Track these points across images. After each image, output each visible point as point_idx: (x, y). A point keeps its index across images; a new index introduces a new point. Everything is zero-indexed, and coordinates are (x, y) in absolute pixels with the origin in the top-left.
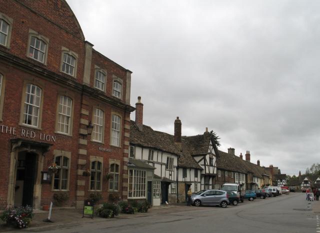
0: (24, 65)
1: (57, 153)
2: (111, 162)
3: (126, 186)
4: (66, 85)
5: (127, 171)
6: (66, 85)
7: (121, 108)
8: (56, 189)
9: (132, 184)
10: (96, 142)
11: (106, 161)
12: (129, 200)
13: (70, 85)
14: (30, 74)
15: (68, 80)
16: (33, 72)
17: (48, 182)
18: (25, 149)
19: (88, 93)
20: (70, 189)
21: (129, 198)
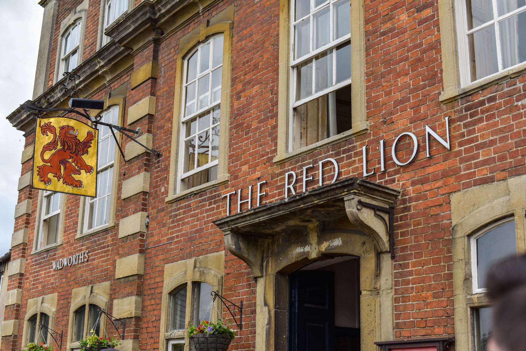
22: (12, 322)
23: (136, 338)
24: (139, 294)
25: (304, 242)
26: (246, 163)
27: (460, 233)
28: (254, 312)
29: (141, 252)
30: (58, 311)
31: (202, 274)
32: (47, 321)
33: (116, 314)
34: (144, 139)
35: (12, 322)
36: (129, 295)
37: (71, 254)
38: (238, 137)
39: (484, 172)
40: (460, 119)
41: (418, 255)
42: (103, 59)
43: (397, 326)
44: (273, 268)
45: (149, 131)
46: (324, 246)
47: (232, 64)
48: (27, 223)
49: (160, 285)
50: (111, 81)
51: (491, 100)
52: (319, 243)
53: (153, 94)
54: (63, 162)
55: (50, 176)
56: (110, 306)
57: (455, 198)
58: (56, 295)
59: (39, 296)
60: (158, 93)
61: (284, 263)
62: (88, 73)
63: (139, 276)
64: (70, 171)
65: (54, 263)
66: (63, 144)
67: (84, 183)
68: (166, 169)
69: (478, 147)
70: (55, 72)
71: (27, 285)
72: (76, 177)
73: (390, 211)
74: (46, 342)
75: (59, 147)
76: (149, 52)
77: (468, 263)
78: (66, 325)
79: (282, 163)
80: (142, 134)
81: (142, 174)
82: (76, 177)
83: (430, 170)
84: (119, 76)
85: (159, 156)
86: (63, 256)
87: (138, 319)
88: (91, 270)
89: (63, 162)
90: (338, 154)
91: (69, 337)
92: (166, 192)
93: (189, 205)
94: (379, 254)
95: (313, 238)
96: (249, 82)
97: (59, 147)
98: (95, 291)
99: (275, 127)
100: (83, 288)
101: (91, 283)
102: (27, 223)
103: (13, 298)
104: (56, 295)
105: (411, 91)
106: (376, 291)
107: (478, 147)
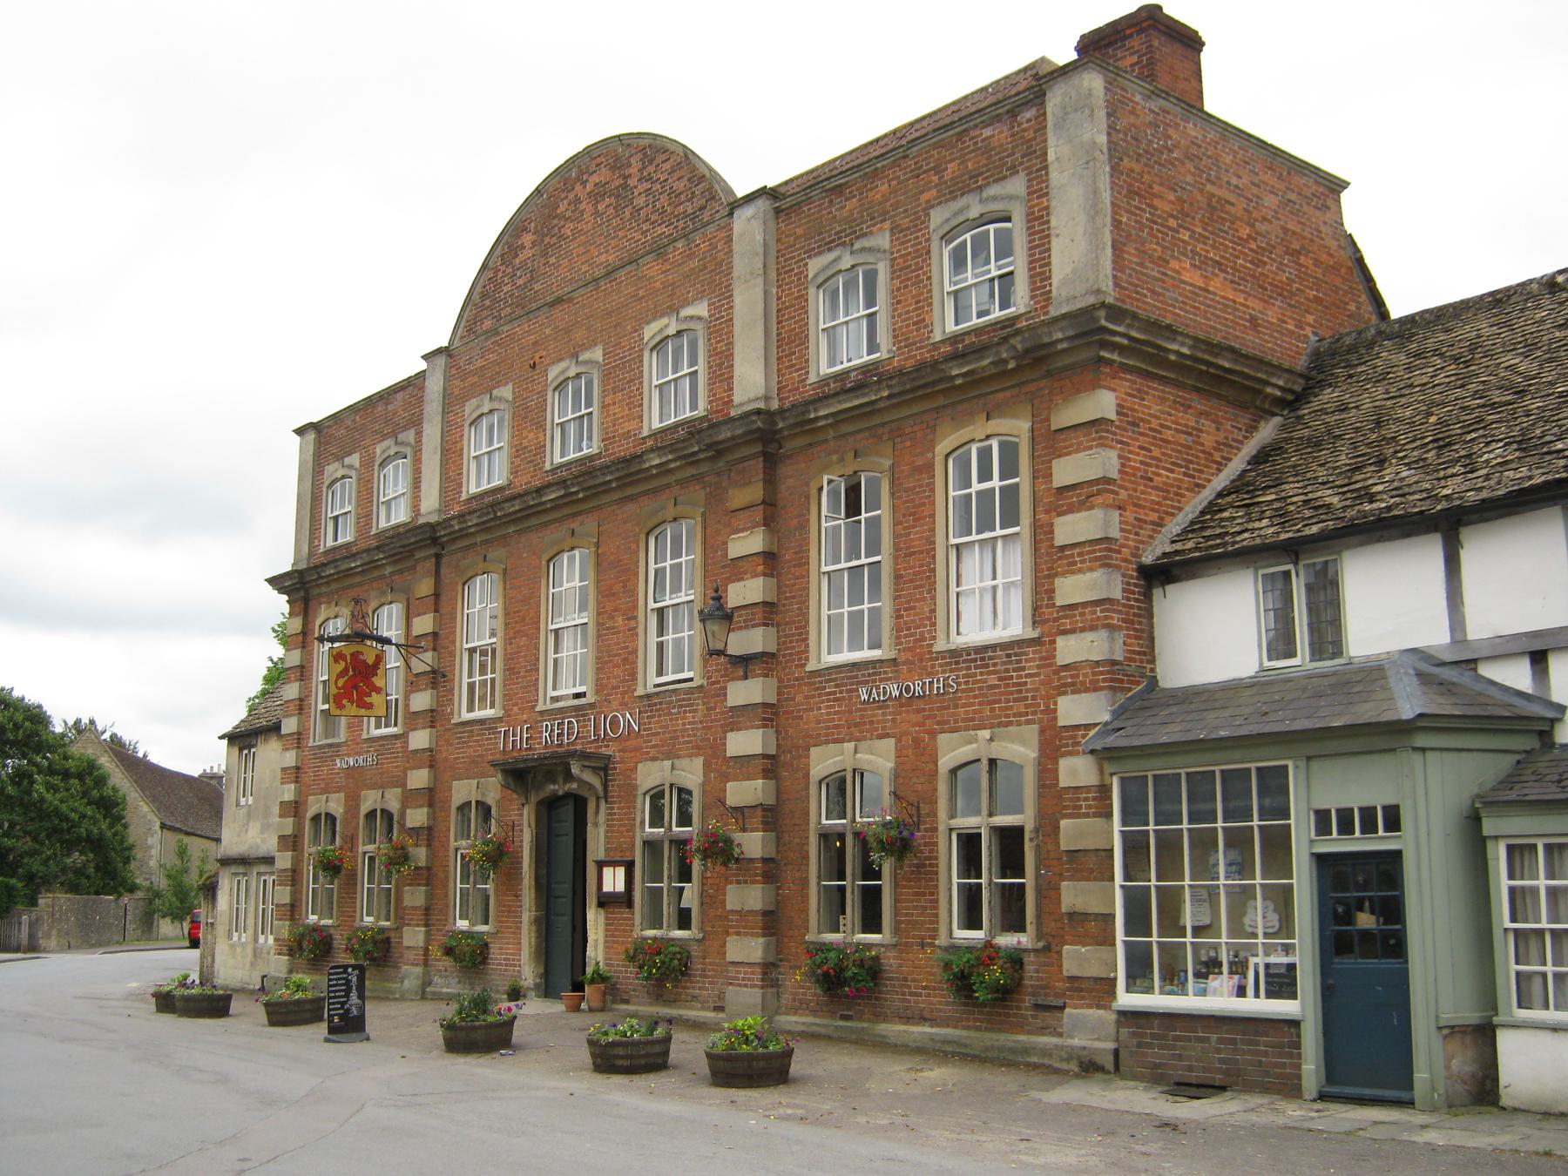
0: (520, 511)
1: (650, 775)
2: (952, 751)
3: (1095, 907)
4: (653, 477)
5: (1104, 791)
6: (653, 477)
7: (1006, 374)
8: (680, 928)
9: (1127, 876)
10: (839, 668)
11: (353, 801)
12: (1131, 1017)
13: (664, 470)
14: (646, 493)
15: (639, 457)
16: (551, 509)
17: (626, 899)
18: (552, 787)
19: (738, 445)
20: (702, 929)
21: (1127, 999)
22: (290, 820)
23: (429, 845)
24: (431, 805)
25: (554, 782)
26: (516, 704)
27: (641, 791)
28: (521, 831)
29: (431, 766)
30: (346, 812)
31: (483, 795)
32: (334, 824)
33: (409, 824)
34: (428, 656)
35: (290, 820)
36: (421, 806)
37: (359, 754)
38: (511, 679)
39: (653, 752)
40: (646, 712)
41: (620, 802)
42: (383, 552)
43: (607, 850)
44: (534, 799)
45: (434, 649)
46: (567, 787)
47: (505, 609)
48: (301, 708)
49: (448, 799)
50: (392, 574)
51: (661, 703)
52: (564, 784)
53: (436, 611)
54: (356, 687)
55: (345, 702)
56: (403, 814)
57: (640, 766)
58: (342, 795)
59: (321, 794)
60: (442, 611)
61: (542, 795)
62: (367, 560)
63: (432, 711)
64: (362, 694)
65: (338, 761)
66: (354, 670)
67: (375, 703)
68: (451, 690)
69: (653, 735)
70: (322, 530)
71: (305, 779)
72: (368, 700)
73: (605, 769)
74: (111, 749)
75: (351, 673)
76: (430, 564)
77: (643, 812)
78: (357, 828)
79: (542, 713)
80: (426, 651)
81: (429, 692)
82: (368, 700)
83: (628, 743)
84: (401, 572)
85: (444, 676)
86: (348, 755)
87: (430, 829)
88: (382, 774)
89: (356, 687)
90: (577, 716)
91: (361, 840)
92: (452, 713)
93: (472, 731)
94: (598, 799)
95: (561, 780)
96: (519, 632)
97: (351, 673)
98: (387, 795)
99: (537, 680)
100: (373, 792)
101: (382, 786)
102: (301, 708)
103: (289, 793)
104: (342, 795)
105: (623, 681)
106: (596, 825)
107: (653, 735)
